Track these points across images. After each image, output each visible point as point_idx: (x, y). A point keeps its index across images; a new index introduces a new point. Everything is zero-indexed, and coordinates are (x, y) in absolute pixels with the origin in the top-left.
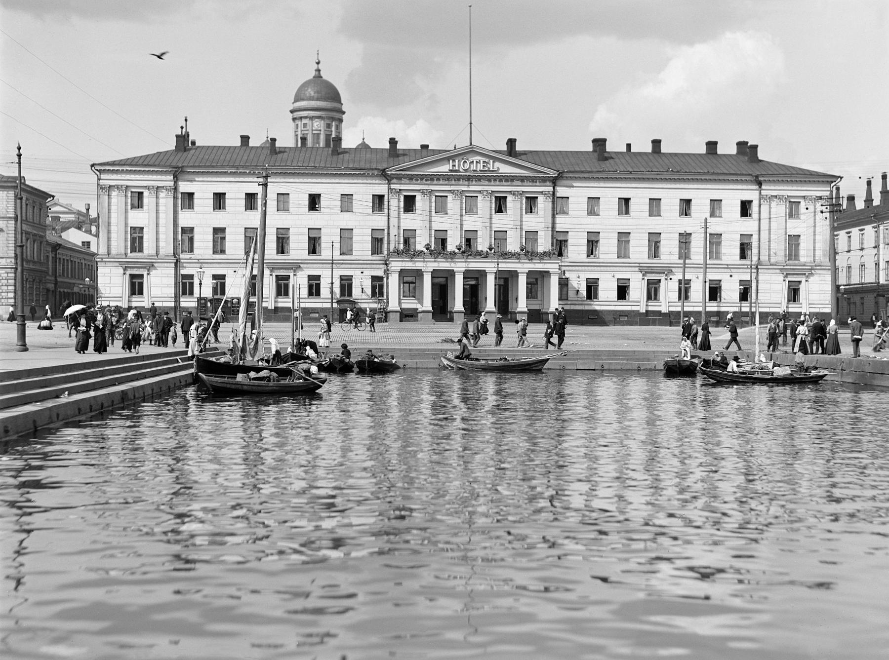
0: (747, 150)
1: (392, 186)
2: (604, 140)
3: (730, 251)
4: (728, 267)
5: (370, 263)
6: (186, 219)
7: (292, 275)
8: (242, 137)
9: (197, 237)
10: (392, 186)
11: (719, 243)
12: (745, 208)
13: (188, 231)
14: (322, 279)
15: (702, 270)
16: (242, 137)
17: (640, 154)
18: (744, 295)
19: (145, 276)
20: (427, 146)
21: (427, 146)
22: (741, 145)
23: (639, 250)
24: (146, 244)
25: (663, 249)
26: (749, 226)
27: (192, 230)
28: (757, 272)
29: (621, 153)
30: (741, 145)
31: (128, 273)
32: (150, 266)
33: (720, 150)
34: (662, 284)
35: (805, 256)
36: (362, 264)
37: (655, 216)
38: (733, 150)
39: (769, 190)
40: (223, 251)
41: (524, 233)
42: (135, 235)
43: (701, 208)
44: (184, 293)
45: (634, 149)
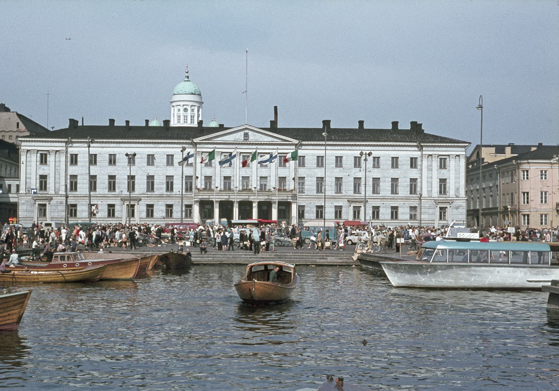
0: (416, 127)
2: (330, 121)
3: (404, 189)
4: (383, 198)
5: (407, 199)
6: (94, 170)
7: (47, 204)
8: (110, 120)
9: (98, 181)
10: (198, 150)
11: (303, 184)
12: (413, 162)
13: (74, 177)
14: (116, 207)
15: (88, 198)
16: (110, 120)
17: (368, 130)
19: (47, 205)
20: (223, 125)
21: (223, 125)
22: (414, 124)
26: (414, 173)
28: (325, 201)
30: (414, 124)
31: (352, 205)
34: (136, 207)
36: (161, 196)
40: (396, 193)
41: (69, 177)
42: (262, 183)
44: (71, 216)
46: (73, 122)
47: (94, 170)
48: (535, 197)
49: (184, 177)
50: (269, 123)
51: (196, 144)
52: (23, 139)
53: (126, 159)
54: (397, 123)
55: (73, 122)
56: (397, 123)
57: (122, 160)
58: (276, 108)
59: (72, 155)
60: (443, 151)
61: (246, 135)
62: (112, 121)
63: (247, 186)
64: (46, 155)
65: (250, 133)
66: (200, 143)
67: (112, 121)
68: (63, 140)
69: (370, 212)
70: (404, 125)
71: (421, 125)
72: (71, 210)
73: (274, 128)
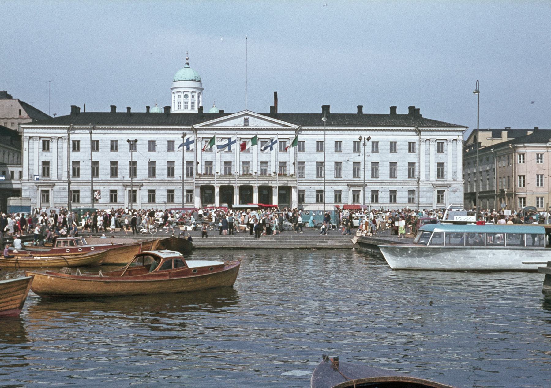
0: (414, 111)
1: (198, 136)
4: (382, 182)
6: (96, 156)
7: (50, 189)
8: (111, 107)
11: (303, 168)
12: (411, 147)
13: (76, 163)
15: (90, 184)
16: (111, 107)
18: (411, 201)
22: (411, 109)
23: (347, 172)
24: (176, 172)
25: (343, 172)
26: (412, 157)
27: (303, 163)
29: (387, 115)
30: (411, 109)
31: (352, 189)
32: (448, 186)
33: (398, 112)
34: (137, 192)
35: (449, 176)
37: (153, 151)
38: (407, 112)
39: (425, 135)
40: (395, 177)
41: (71, 163)
42: (262, 168)
43: (142, 147)
44: (74, 201)
45: (365, 112)
46: (75, 109)
47: (96, 156)
48: (531, 180)
49: (185, 162)
50: (390, 110)
51: (196, 130)
52: (25, 126)
53: (127, 145)
54: (328, 107)
55: (75, 109)
56: (328, 107)
57: (124, 146)
58: (276, 94)
59: (74, 142)
60: (441, 136)
61: (246, 121)
62: (113, 108)
63: (248, 170)
64: (48, 141)
65: (250, 119)
66: (200, 129)
67: (113, 108)
68: (65, 127)
69: (369, 195)
70: (402, 110)
71: (419, 109)
72: (74, 196)
73: (274, 113)
